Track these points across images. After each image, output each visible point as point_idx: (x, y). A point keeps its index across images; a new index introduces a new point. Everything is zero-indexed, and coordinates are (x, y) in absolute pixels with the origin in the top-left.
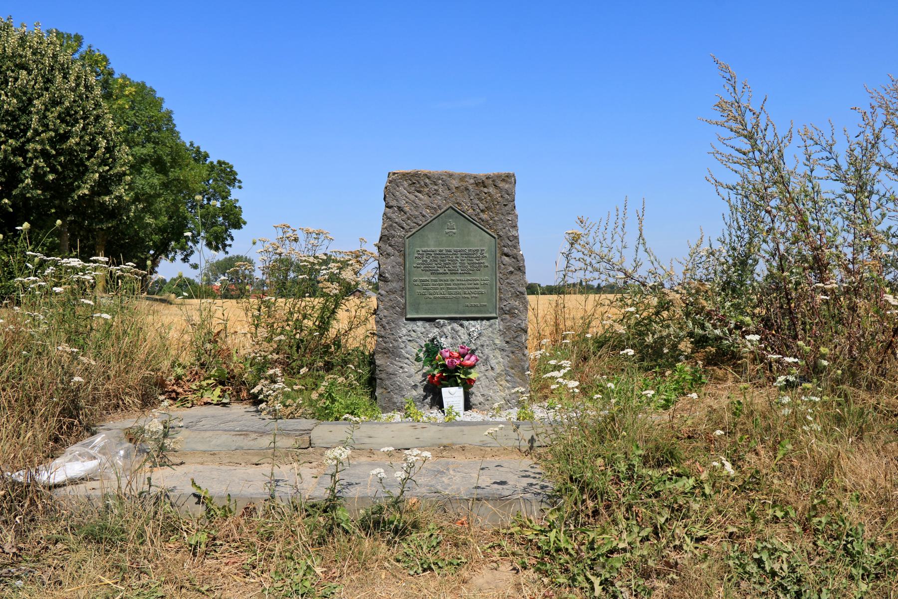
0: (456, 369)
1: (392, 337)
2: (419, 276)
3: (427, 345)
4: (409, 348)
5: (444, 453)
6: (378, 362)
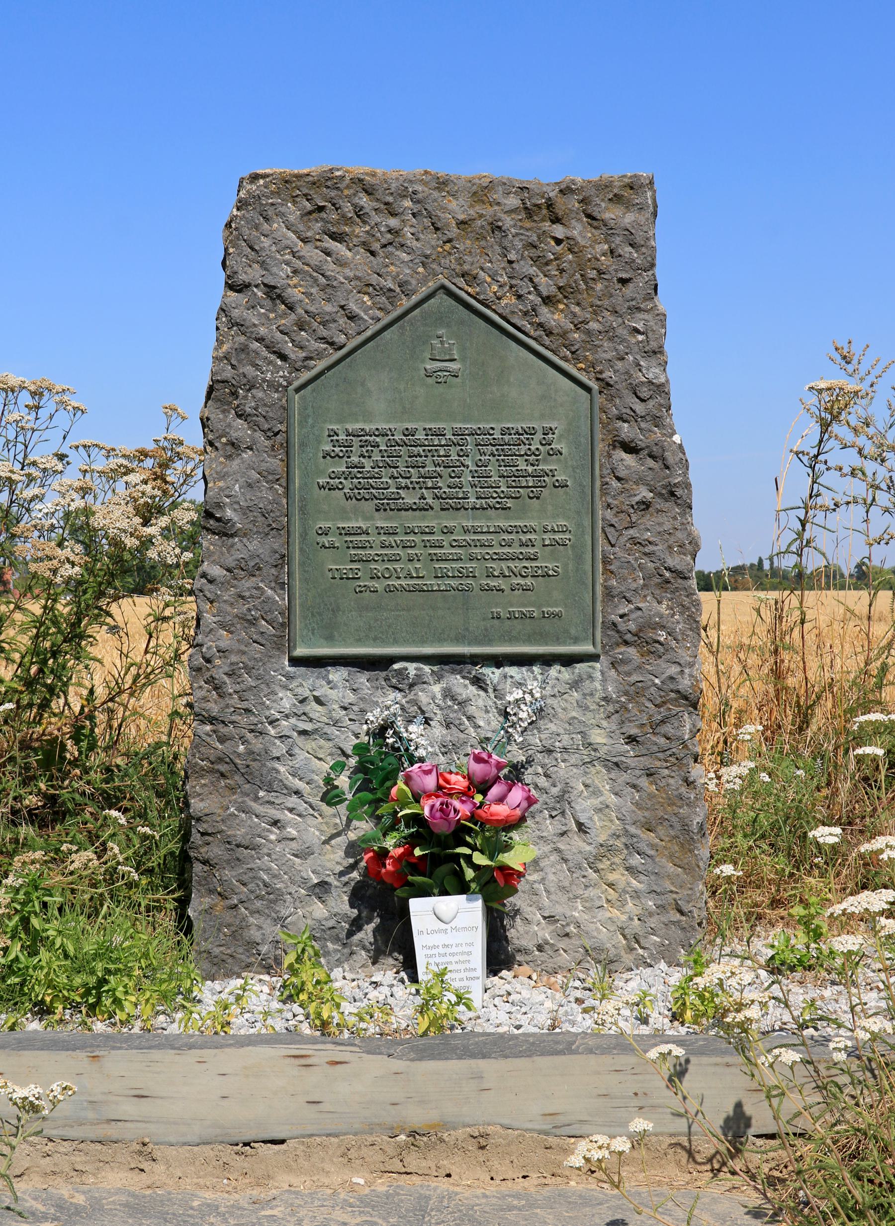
0: (459, 834)
1: (243, 720)
2: (338, 515)
3: (361, 749)
4: (301, 756)
5: (413, 1161)
6: (197, 806)
